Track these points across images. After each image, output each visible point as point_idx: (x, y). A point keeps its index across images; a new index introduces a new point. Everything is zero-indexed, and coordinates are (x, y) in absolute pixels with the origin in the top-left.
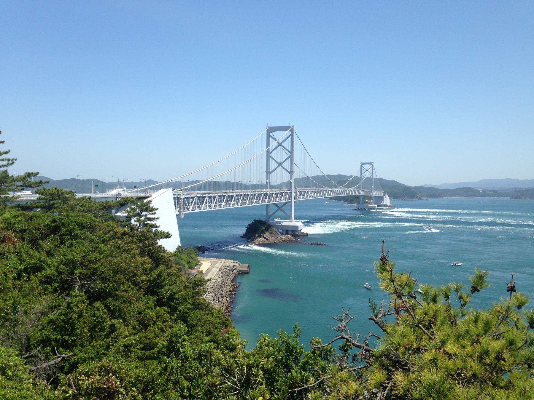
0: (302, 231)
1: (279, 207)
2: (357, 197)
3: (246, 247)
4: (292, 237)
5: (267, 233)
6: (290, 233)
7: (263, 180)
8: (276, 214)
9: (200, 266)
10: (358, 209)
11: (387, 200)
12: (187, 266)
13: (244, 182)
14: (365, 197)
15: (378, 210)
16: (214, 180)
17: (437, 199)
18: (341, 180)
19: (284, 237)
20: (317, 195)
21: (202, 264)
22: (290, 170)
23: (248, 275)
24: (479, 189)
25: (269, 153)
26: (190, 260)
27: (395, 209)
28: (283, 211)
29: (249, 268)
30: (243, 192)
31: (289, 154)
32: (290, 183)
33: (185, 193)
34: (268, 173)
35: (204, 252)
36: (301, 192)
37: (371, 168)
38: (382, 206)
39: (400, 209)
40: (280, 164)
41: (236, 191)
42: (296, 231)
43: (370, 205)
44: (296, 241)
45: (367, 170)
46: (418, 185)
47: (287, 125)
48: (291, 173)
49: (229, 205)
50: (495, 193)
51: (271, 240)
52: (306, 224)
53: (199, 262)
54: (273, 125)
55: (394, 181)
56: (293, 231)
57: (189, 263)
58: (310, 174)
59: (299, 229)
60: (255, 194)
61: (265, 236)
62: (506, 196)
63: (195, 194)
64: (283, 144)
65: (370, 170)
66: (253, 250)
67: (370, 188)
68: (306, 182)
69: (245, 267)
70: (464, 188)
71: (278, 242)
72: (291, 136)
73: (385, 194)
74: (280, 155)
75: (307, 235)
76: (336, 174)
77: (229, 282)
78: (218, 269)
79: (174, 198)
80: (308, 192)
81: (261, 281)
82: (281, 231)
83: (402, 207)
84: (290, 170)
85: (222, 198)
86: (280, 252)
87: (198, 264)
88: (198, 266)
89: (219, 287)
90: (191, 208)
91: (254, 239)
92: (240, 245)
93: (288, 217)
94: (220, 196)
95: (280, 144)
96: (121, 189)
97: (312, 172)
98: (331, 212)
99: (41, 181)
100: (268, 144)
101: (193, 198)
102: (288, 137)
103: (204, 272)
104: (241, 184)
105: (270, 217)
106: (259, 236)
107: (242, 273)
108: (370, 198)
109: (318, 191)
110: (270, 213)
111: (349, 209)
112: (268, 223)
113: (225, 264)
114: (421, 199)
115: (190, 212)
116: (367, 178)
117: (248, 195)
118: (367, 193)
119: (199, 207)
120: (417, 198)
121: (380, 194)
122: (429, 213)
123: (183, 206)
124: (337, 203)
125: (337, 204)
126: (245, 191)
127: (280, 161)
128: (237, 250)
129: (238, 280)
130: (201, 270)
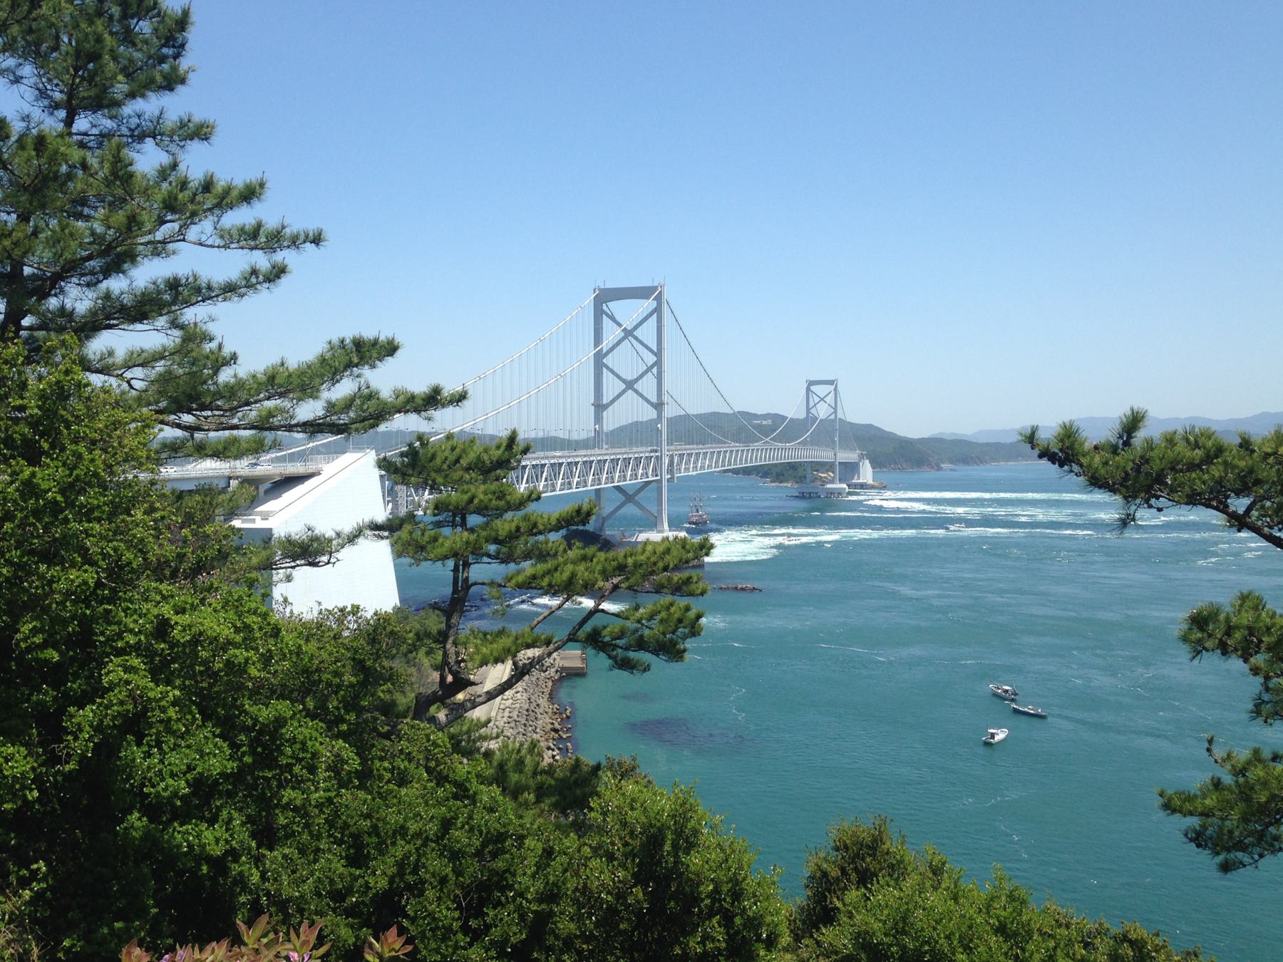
1: (627, 496)
2: (793, 467)
7: (582, 426)
10: (802, 496)
11: (867, 473)
15: (850, 498)
18: (742, 428)
22: (654, 400)
25: (599, 359)
27: (888, 494)
31: (651, 359)
34: (600, 407)
36: (681, 456)
39: (901, 494)
40: (630, 385)
43: (829, 486)
48: (659, 406)
54: (611, 284)
55: (871, 426)
65: (830, 399)
67: (831, 444)
72: (658, 311)
74: (627, 361)
77: (543, 702)
83: (906, 489)
84: (654, 400)
89: (523, 721)
92: (541, 595)
93: (653, 524)
95: (628, 333)
99: (436, 391)
108: (829, 467)
109: (705, 454)
111: (774, 495)
114: (939, 469)
118: (824, 455)
121: (851, 456)
124: (743, 481)
127: (629, 377)
128: (533, 608)
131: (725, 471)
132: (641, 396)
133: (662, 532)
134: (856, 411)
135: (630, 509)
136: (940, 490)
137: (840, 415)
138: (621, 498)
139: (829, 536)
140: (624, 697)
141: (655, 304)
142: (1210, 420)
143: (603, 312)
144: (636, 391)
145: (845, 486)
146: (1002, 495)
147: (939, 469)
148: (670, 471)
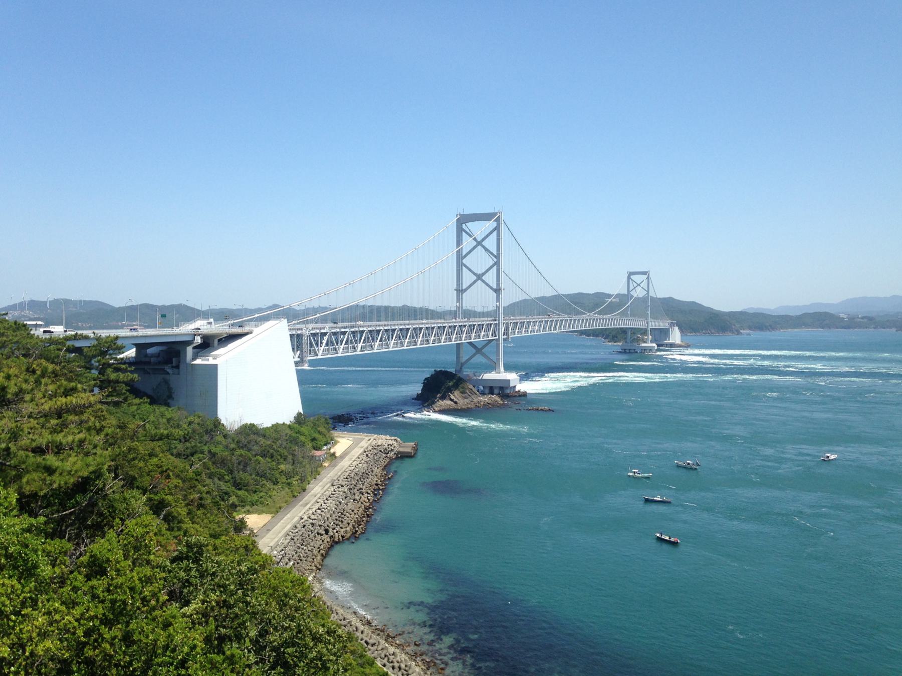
0: (517, 389)
1: (477, 349)
2: (624, 331)
3: (418, 416)
5: (457, 393)
6: (496, 391)
7: (449, 302)
8: (472, 361)
9: (334, 445)
10: (624, 351)
11: (676, 336)
13: (432, 308)
14: (634, 331)
15: (658, 353)
17: (768, 333)
19: (485, 399)
21: (337, 442)
22: (495, 287)
23: (413, 459)
24: (842, 315)
25: (460, 257)
26: (316, 435)
27: (690, 351)
29: (416, 449)
31: (464, 261)
33: (311, 326)
34: (460, 291)
37: (646, 281)
38: (667, 345)
39: (697, 351)
40: (479, 277)
42: (507, 388)
43: (643, 345)
44: (503, 406)
46: (738, 309)
48: (497, 291)
49: (388, 346)
50: (871, 322)
51: (462, 403)
52: (525, 378)
54: (468, 211)
55: (694, 303)
56: (501, 388)
57: (314, 439)
60: (455, 327)
61: (452, 397)
62: (890, 328)
65: (644, 285)
66: (430, 420)
68: (527, 308)
69: (408, 447)
71: (473, 406)
72: (497, 229)
73: (672, 325)
74: (479, 261)
75: (524, 395)
76: (591, 292)
77: (377, 471)
79: (291, 336)
80: (529, 323)
82: (481, 387)
84: (495, 287)
86: (474, 423)
88: (329, 446)
90: (321, 352)
91: (434, 403)
93: (493, 367)
96: (205, 322)
100: (459, 242)
101: (325, 334)
102: (491, 232)
103: (337, 455)
104: (427, 310)
105: (462, 364)
106: (443, 398)
108: (644, 332)
109: (557, 321)
110: (464, 359)
111: (607, 349)
112: (460, 375)
113: (373, 444)
114: (739, 333)
115: (319, 357)
116: (637, 299)
117: (444, 327)
118: (639, 324)
121: (663, 324)
123: (306, 347)
126: (401, 322)
127: (479, 272)
129: (393, 468)
130: (332, 451)
132: (487, 285)
134: (661, 291)
135: (479, 359)
138: (474, 351)
140: (430, 469)
141: (495, 224)
144: (483, 281)
145: (654, 345)
148: (506, 333)
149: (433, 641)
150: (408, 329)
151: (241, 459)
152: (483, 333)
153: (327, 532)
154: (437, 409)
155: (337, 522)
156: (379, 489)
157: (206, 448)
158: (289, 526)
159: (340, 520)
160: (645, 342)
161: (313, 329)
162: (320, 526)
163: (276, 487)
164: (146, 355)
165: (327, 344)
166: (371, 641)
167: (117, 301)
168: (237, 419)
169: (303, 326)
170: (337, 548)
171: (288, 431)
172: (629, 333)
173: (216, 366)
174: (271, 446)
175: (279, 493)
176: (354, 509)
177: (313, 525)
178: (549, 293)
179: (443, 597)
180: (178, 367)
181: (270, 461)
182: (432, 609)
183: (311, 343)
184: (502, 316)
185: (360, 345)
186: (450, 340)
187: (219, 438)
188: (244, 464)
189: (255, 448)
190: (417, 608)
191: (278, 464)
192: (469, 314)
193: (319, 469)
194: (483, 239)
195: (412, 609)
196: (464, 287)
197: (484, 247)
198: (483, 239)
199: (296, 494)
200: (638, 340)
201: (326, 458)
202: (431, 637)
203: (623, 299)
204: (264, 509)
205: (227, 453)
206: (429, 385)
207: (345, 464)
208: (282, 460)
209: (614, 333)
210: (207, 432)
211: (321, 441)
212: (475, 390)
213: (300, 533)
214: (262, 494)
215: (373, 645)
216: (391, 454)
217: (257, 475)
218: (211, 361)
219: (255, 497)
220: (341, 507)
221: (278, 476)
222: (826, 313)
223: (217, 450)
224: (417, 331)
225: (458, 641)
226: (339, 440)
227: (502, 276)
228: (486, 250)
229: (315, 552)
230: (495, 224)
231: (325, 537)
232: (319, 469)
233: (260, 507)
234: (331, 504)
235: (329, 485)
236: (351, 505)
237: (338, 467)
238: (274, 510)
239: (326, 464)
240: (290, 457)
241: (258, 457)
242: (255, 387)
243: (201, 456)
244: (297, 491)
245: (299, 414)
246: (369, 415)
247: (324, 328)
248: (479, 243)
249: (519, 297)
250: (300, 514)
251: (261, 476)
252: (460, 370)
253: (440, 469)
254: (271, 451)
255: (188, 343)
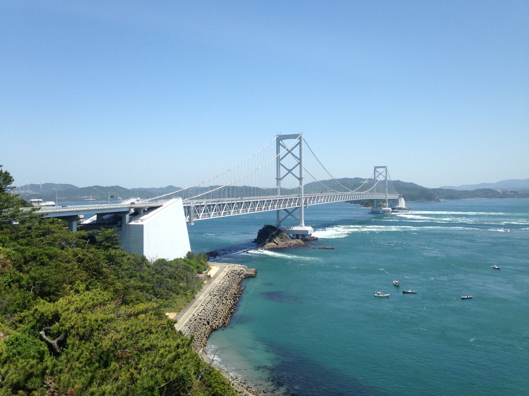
0: (312, 236)
2: (372, 201)
3: (256, 252)
4: (302, 242)
5: (278, 238)
6: (300, 237)
7: (272, 184)
9: (209, 270)
10: (373, 213)
11: (402, 203)
12: (196, 271)
14: (378, 201)
15: (393, 213)
16: (233, 185)
18: (354, 184)
19: (294, 242)
20: (327, 200)
21: (211, 269)
22: (299, 177)
24: (499, 190)
25: (279, 160)
26: (199, 265)
27: (410, 212)
28: (293, 216)
29: (256, 272)
30: (259, 199)
31: (281, 162)
32: (300, 189)
33: (195, 201)
34: (279, 179)
35: (215, 257)
37: (385, 172)
38: (397, 209)
39: (413, 212)
40: (290, 171)
41: (244, 198)
42: (306, 235)
43: (295, 228)
44: (304, 246)
45: (381, 174)
46: (437, 187)
47: (296, 133)
48: (300, 179)
49: (238, 212)
50: (515, 194)
51: (281, 244)
53: (208, 267)
55: (399, 181)
56: (303, 235)
57: (198, 267)
58: (319, 179)
59: (309, 234)
60: (276, 200)
61: (275, 241)
63: (204, 202)
64: (292, 152)
67: (384, 192)
69: (251, 272)
70: (483, 190)
71: (287, 246)
72: (300, 143)
73: (400, 197)
74: (289, 162)
75: (316, 239)
76: (352, 177)
77: (235, 286)
78: (226, 273)
79: (184, 207)
81: (268, 284)
82: (291, 235)
83: (424, 210)
84: (299, 177)
85: (231, 205)
87: (207, 268)
88: (207, 271)
91: (265, 244)
92: (251, 249)
93: (298, 224)
94: (238, 203)
97: (321, 176)
98: (343, 215)
100: (278, 151)
101: (203, 206)
102: (296, 145)
103: (211, 276)
105: (280, 222)
106: (270, 241)
107: (248, 277)
108: (384, 201)
109: (334, 196)
110: (280, 219)
111: (363, 212)
112: (279, 228)
114: (439, 201)
118: (381, 197)
119: (209, 214)
120: (434, 200)
122: (446, 216)
123: (192, 213)
125: (354, 208)
127: (290, 168)
129: (244, 283)
130: (209, 274)
131: (347, 202)
132: (294, 175)
133: (302, 226)
134: (394, 176)
136: (437, 211)
137: (388, 179)
139: (382, 228)
141: (299, 141)
142: (489, 184)
143: (280, 144)
144: (292, 174)
145: (390, 209)
146: (467, 213)
147: (439, 201)
148: (305, 203)
149: (274, 390)
150: (250, 202)
151: (158, 280)
152: (292, 204)
153: (208, 323)
154: (266, 248)
155: (214, 317)
156: (236, 297)
157: (138, 274)
158: (187, 320)
159: (215, 316)
160: (384, 207)
161: (196, 203)
162: (204, 320)
163: (178, 296)
164: (103, 220)
165: (204, 212)
166: (239, 390)
167: (81, 183)
168: (155, 256)
169: (190, 201)
170: (215, 333)
171: (183, 263)
172: (375, 202)
173: (142, 226)
174: (174, 272)
175: (180, 300)
176: (223, 309)
177: (200, 319)
178: (328, 178)
179: (277, 363)
180: (121, 226)
181: (174, 280)
182: (272, 370)
183: (195, 211)
184: (303, 193)
185: (223, 212)
186: (274, 208)
187: (145, 268)
188: (160, 283)
189: (166, 273)
190: (263, 369)
191: (179, 283)
192: (284, 192)
193: (202, 285)
194: (292, 149)
195: (261, 370)
196: (281, 177)
197: (292, 154)
198: (292, 149)
199: (190, 300)
200: (380, 206)
201: (205, 278)
202: (272, 388)
203: (372, 182)
204: (172, 309)
205: (150, 277)
206: (261, 233)
207: (216, 281)
208: (181, 280)
209: (366, 202)
210: (138, 264)
211: (202, 268)
212: (288, 236)
213: (194, 324)
214: (170, 301)
215: (240, 393)
216: (242, 276)
217: (168, 289)
218: (139, 223)
219: (167, 303)
220: (215, 308)
221: (179, 290)
222: (489, 189)
223: (145, 275)
224: (255, 203)
225: (288, 390)
226: (212, 267)
227: (303, 170)
228: (293, 155)
229: (203, 335)
230: (299, 141)
231: (207, 326)
232: (202, 285)
233: (170, 309)
234: (210, 306)
235: (208, 295)
236: (221, 307)
237: (212, 284)
238: (177, 310)
239: (205, 282)
240: (185, 278)
241: (168, 279)
242: (165, 237)
243: (136, 278)
244: (190, 298)
245: (189, 253)
246: (228, 252)
247: (202, 202)
248: (290, 152)
249: (312, 180)
250: (193, 313)
251: (170, 290)
252: (279, 225)
253: (270, 284)
254: (175, 275)
255: (126, 213)
